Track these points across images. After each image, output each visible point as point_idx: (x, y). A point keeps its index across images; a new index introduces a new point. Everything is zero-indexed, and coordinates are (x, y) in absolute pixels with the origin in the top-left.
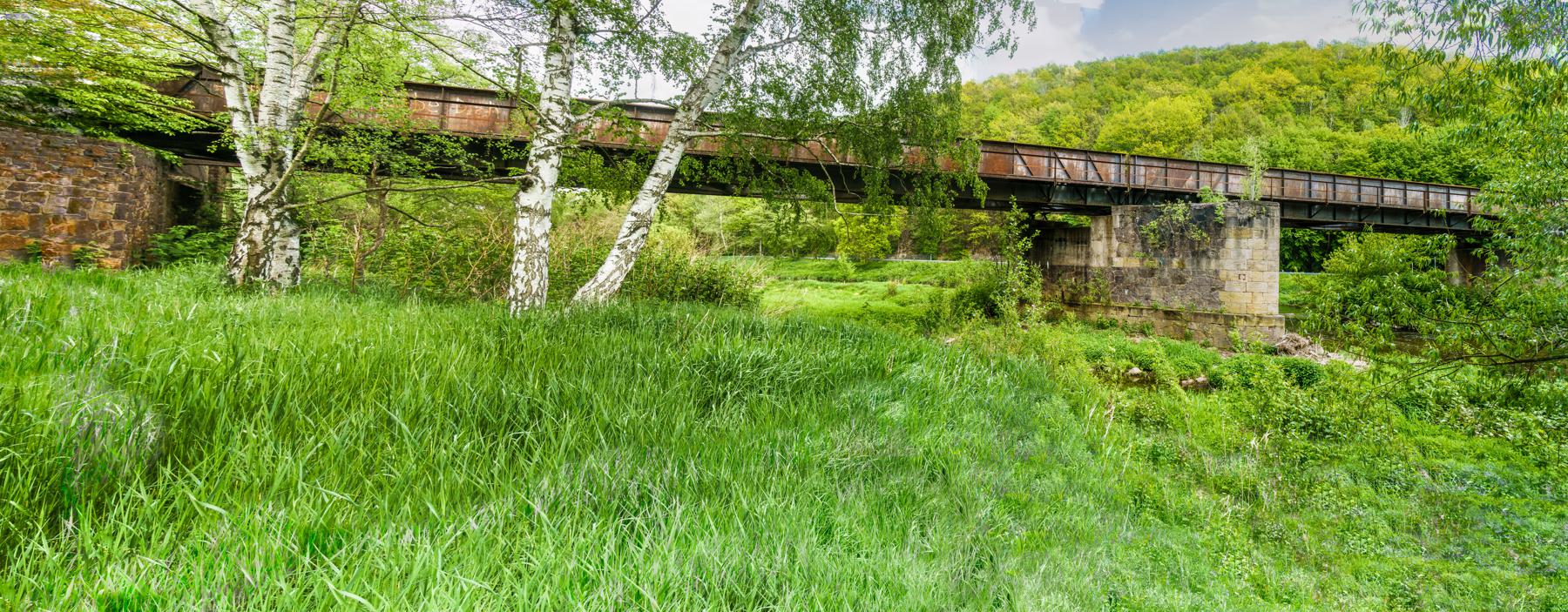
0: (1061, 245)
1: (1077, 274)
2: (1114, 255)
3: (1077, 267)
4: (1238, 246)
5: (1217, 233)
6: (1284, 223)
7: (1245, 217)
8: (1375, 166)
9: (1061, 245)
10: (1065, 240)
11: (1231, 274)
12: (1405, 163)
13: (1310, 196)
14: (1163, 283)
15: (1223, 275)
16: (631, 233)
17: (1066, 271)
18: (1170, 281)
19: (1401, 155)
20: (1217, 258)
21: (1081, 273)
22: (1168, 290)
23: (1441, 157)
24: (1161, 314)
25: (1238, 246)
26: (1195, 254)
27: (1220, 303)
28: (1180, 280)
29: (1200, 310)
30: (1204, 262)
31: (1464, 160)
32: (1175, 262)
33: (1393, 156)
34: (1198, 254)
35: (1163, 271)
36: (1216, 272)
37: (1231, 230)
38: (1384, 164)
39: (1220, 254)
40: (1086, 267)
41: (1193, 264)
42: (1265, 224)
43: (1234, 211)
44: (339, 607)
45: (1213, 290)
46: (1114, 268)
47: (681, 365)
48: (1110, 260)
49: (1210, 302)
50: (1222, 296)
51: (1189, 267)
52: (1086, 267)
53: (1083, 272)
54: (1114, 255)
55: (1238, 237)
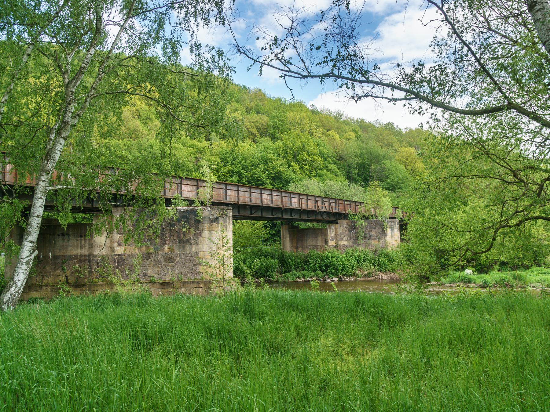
0: (63, 239)
1: (80, 261)
2: (115, 245)
3: (81, 256)
4: (211, 234)
5: (196, 228)
6: (235, 218)
7: (214, 216)
8: (224, 169)
9: (63, 239)
10: (69, 235)
11: (207, 254)
12: (243, 168)
13: (226, 199)
14: (157, 263)
15: (201, 254)
16: (31, 254)
17: (70, 259)
18: (163, 262)
19: (240, 162)
20: (197, 244)
21: (85, 260)
22: (161, 268)
23: (263, 165)
24: (158, 285)
25: (211, 234)
26: (181, 242)
27: (199, 273)
28: (171, 260)
29: (185, 279)
30: (188, 247)
31: (276, 168)
32: (166, 248)
33: (235, 162)
34: (183, 242)
35: (156, 255)
36: (197, 253)
37: (206, 225)
38: (231, 168)
39: (199, 241)
40: (90, 255)
41: (180, 249)
42: (225, 221)
43: (207, 213)
44: (301, 410)
45: (194, 265)
46: (116, 255)
47: (111, 340)
48: (112, 249)
49: (193, 274)
50: (201, 269)
51: (177, 251)
52: (90, 255)
53: (88, 259)
54: (115, 245)
55: (211, 230)
